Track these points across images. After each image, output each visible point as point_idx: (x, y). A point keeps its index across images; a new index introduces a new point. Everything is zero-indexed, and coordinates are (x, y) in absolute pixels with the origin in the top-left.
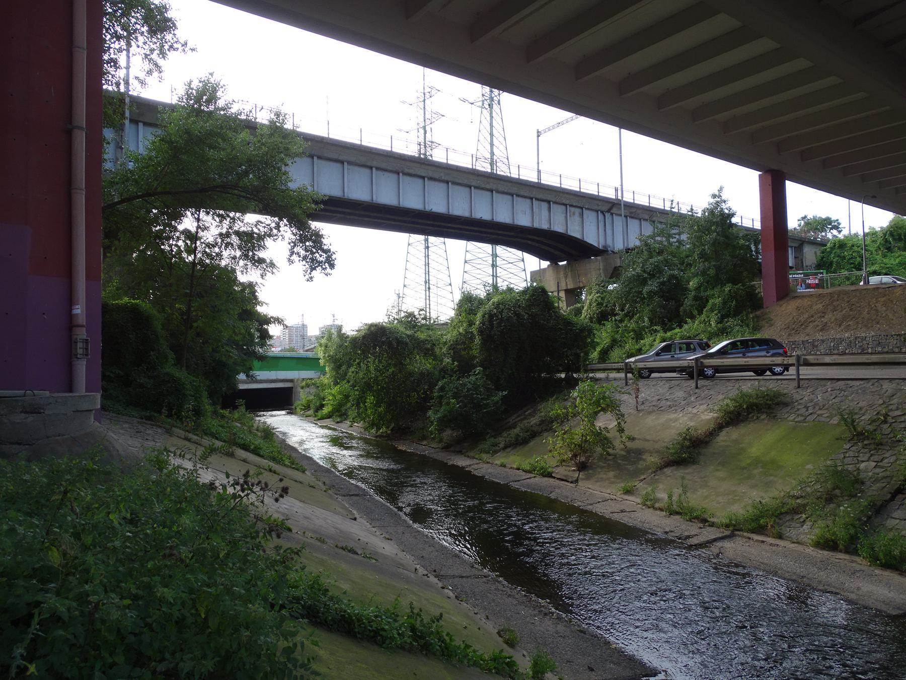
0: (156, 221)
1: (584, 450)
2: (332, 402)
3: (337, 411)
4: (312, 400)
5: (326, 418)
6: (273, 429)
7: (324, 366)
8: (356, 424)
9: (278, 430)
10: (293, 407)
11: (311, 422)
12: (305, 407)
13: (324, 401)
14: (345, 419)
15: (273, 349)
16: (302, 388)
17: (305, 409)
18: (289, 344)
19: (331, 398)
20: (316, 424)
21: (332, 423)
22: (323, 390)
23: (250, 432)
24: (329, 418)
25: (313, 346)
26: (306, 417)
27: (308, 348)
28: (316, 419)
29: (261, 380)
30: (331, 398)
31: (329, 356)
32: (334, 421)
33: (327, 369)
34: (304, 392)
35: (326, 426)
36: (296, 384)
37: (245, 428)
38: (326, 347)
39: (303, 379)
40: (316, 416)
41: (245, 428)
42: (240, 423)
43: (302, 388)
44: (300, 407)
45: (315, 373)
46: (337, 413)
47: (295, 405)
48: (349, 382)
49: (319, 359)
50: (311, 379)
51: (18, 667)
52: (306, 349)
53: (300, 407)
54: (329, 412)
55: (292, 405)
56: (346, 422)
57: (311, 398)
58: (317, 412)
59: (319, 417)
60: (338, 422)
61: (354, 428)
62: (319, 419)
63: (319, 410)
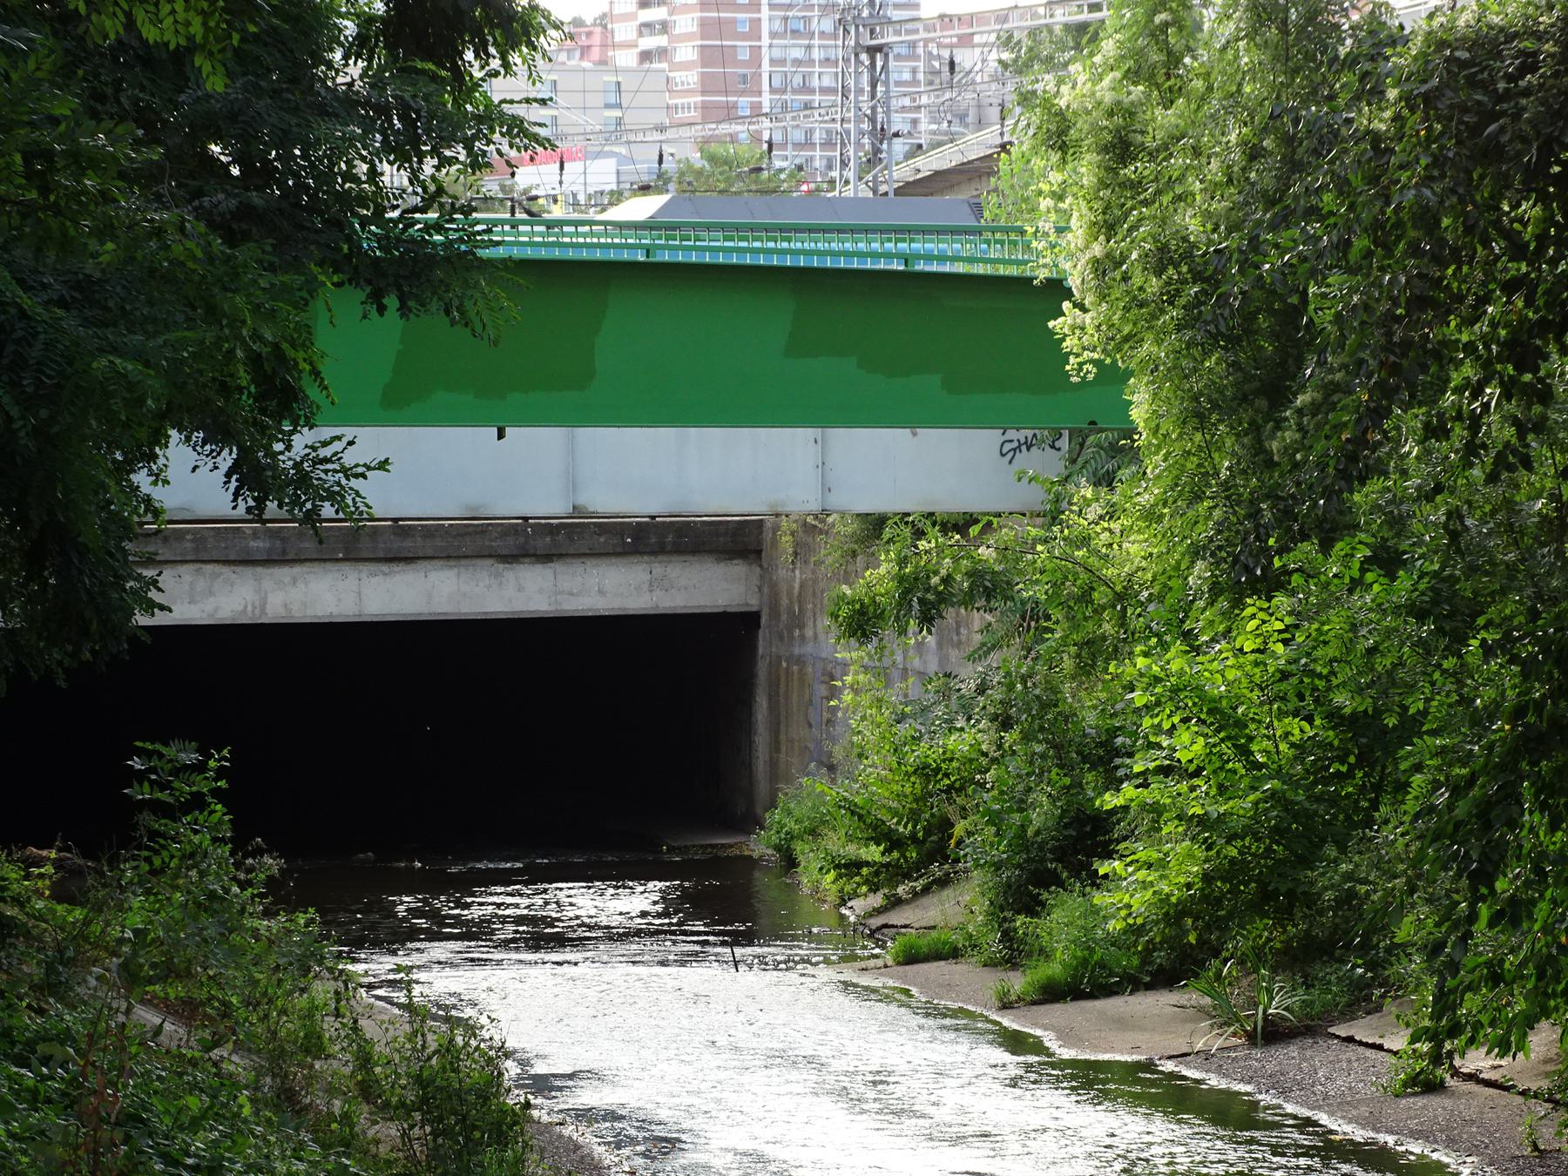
0: (1428, 1065)
1: (1550, 599)
2: (1199, 800)
3: (1265, 900)
4: (978, 762)
5: (1133, 983)
6: (543, 1085)
7: (1112, 377)
8: (1477, 1060)
9: (587, 1096)
10: (760, 846)
11: (961, 1020)
12: (893, 842)
13: (1114, 784)
14: (1360, 1001)
15: (534, 177)
16: (862, 623)
17: (898, 873)
18: (708, 112)
19: (1189, 745)
20: (1015, 1042)
21: (1206, 1039)
22: (1093, 654)
23: (287, 1101)
24: (1165, 979)
25: (975, 145)
26: (911, 958)
27: (928, 164)
28: (1018, 982)
29: (399, 528)
30: (1189, 745)
31: (1161, 260)
32: (1224, 1017)
33: (1140, 406)
34: (884, 675)
35: (1132, 1071)
36: (792, 577)
37: (237, 1064)
38: (1121, 148)
39: (875, 525)
40: (1014, 954)
41: (237, 1064)
42: (187, 1011)
43: (862, 623)
44: (838, 843)
45: (1010, 452)
46: (1262, 930)
47: (781, 819)
48: (1387, 561)
49: (1057, 290)
50: (959, 524)
51: (1090, 12)
52: (903, 172)
53: (838, 843)
54: (1174, 914)
55: (749, 822)
56: (1361, 1029)
57: (959, 743)
58: (1033, 907)
59: (1054, 969)
60: (1272, 1034)
61: (1466, 1102)
62: (1051, 993)
63: (1049, 880)
